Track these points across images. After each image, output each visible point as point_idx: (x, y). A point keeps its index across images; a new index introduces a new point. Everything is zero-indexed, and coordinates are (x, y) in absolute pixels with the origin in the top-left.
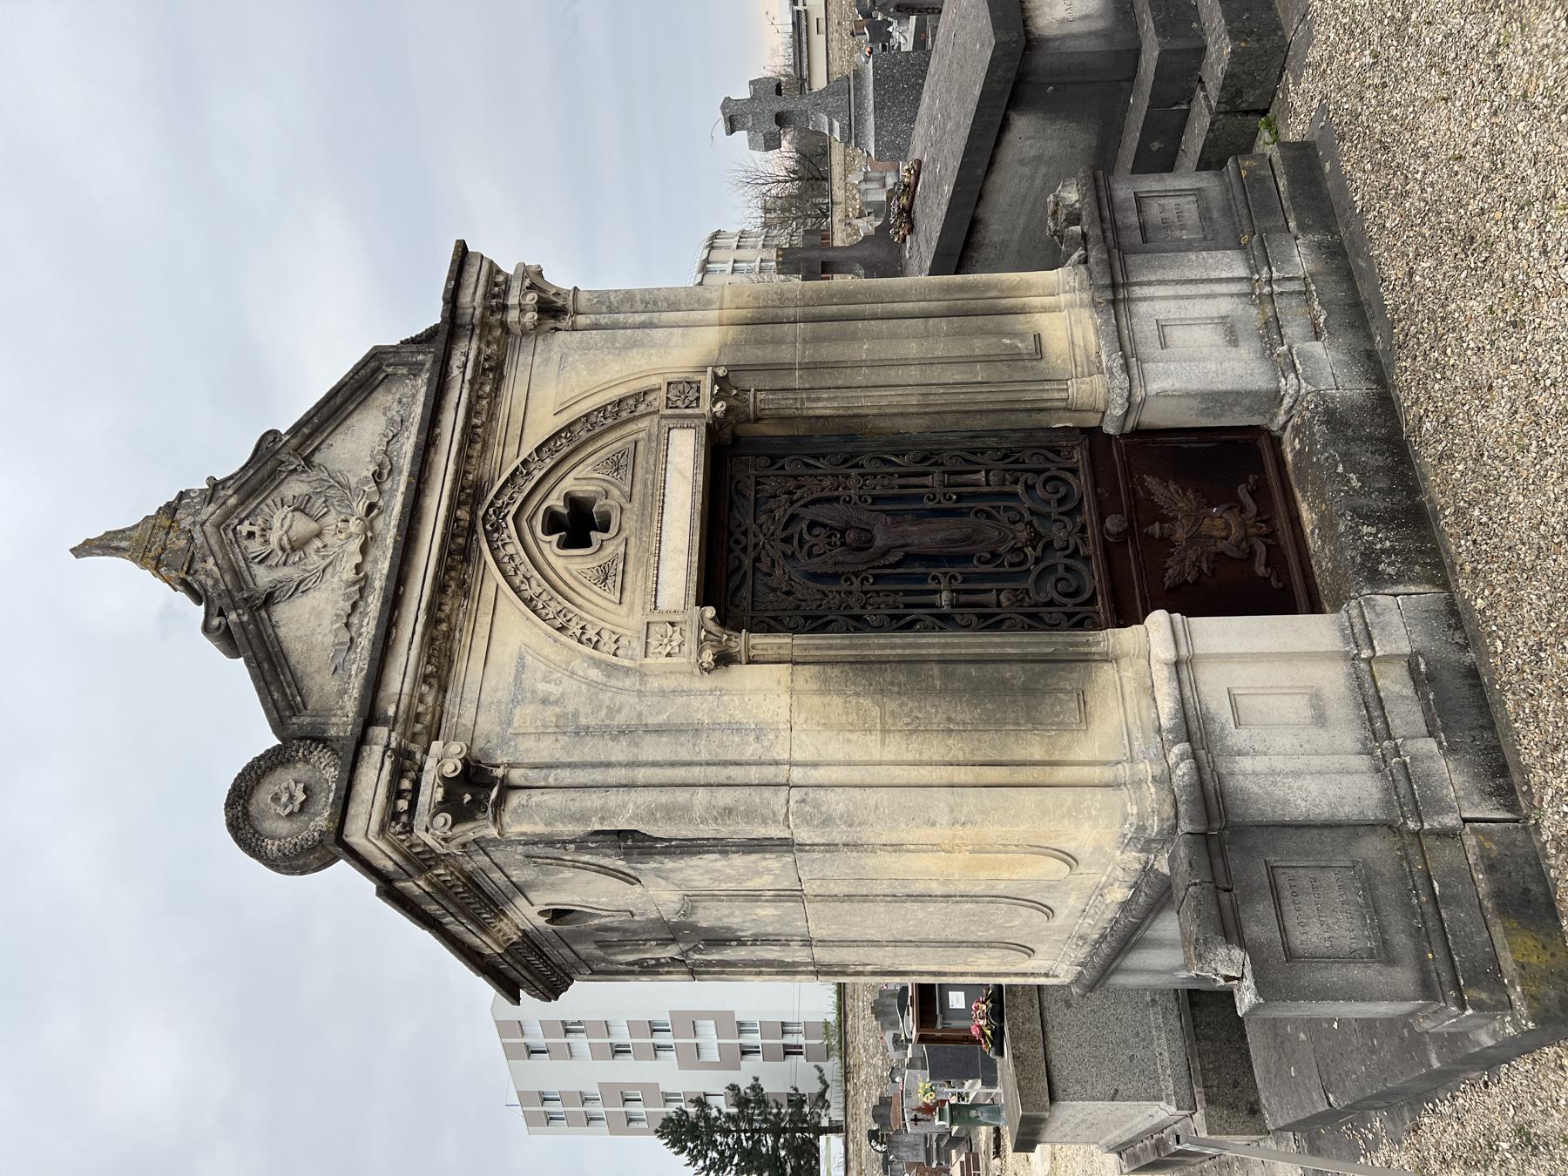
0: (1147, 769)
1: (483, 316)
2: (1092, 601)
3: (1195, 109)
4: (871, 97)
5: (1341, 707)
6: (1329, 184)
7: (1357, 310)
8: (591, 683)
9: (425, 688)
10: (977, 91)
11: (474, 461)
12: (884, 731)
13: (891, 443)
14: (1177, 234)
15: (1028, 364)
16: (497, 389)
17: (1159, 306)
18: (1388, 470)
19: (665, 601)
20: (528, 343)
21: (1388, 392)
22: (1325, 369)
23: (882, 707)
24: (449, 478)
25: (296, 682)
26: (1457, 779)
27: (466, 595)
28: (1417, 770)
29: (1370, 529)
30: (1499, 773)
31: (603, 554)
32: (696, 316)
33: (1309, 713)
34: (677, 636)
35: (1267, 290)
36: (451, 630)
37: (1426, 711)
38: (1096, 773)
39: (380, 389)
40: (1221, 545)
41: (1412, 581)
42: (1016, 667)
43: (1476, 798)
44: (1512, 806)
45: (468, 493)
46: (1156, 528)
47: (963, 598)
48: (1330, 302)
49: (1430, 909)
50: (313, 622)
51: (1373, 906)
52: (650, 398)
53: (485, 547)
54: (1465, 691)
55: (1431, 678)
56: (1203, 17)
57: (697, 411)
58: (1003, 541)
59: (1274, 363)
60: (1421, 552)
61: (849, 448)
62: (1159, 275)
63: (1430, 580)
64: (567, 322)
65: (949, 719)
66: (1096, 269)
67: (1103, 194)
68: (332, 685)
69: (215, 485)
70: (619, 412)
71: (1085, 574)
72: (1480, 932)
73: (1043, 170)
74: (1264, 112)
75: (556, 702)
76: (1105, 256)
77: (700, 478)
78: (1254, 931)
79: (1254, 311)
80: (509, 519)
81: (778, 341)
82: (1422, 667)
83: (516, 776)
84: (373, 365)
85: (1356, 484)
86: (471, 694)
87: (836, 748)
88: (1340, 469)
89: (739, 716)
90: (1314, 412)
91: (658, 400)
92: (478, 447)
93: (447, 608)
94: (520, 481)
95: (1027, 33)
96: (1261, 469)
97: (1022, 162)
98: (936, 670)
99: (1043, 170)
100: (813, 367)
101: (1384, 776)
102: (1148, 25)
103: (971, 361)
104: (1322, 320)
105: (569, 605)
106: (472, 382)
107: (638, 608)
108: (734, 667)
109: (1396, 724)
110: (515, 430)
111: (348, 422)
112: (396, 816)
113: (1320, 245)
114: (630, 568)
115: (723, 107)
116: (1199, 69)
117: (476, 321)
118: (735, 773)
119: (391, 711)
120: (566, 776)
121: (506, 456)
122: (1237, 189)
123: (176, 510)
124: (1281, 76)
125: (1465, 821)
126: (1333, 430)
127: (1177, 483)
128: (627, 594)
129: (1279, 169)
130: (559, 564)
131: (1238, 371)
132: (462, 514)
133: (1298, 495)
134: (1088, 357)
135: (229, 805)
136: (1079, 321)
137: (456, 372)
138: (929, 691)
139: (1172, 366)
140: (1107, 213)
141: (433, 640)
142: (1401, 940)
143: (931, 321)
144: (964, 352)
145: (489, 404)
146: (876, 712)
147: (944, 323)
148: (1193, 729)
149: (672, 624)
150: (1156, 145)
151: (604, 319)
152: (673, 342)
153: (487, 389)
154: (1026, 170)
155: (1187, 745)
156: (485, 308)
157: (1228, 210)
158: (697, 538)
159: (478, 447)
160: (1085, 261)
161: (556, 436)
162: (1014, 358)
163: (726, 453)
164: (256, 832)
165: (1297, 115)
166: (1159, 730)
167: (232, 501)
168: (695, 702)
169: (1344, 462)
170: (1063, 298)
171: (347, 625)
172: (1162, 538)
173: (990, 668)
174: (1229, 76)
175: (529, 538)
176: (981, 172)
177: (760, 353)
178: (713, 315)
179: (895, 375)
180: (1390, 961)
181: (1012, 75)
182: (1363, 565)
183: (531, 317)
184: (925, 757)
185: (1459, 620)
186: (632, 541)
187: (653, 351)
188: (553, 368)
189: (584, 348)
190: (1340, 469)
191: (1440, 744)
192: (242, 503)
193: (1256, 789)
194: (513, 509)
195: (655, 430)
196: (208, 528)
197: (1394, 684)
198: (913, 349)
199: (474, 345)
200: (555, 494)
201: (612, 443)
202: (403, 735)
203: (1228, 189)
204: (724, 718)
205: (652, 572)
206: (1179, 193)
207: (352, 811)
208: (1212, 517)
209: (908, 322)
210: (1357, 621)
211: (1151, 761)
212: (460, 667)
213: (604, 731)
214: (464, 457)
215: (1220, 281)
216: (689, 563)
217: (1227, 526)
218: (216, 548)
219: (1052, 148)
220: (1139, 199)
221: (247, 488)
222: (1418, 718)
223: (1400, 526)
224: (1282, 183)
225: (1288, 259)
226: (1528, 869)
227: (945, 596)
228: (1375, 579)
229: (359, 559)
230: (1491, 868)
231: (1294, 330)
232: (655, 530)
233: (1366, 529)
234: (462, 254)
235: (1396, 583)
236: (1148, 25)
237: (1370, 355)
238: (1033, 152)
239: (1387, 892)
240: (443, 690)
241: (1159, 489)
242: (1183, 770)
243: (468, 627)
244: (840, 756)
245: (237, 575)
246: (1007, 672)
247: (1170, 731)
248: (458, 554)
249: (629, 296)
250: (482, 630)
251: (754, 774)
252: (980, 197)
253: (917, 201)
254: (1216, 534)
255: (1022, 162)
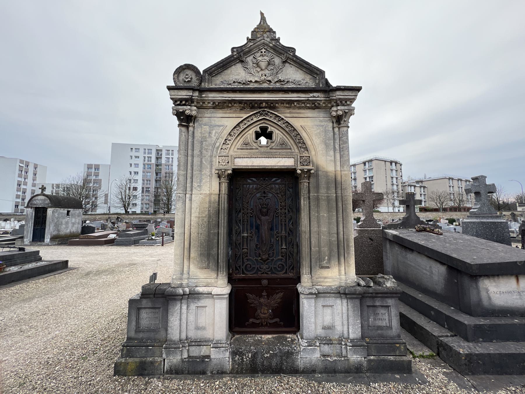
0: (185, 282)
1: (333, 99)
2: (243, 273)
3: (444, 330)
4: (488, 221)
5: (200, 335)
6: (390, 375)
7: (331, 371)
8: (215, 144)
9: (212, 103)
10: (454, 255)
11: (282, 105)
12: (199, 217)
13: (296, 222)
14: (372, 317)
15: (318, 264)
16: (309, 108)
17: (340, 307)
18: (270, 366)
19: (237, 160)
20: (328, 115)
21: (299, 373)
22: (308, 356)
23: (205, 217)
24: (274, 99)
25: (219, 73)
26: (175, 361)
27: (241, 110)
28: (178, 351)
29: (250, 356)
30: (176, 372)
31: (253, 143)
32: (338, 163)
33: (201, 326)
34: (224, 164)
35: (343, 343)
36: (230, 107)
37: (196, 357)
38: (186, 269)
39: (311, 77)
40: (259, 311)
41: (233, 364)
42: (216, 252)
43: (170, 364)
44: (167, 373)
45: (272, 105)
46: (264, 294)
47: (245, 239)
48: (336, 363)
49: (145, 345)
50: (237, 74)
51: (149, 330)
52: (306, 152)
53: (255, 112)
54: (199, 369)
55: (203, 361)
56: (484, 344)
57: (299, 165)
58: (263, 252)
59: (313, 340)
60: (242, 369)
61: (294, 210)
62: (350, 309)
63: (233, 369)
64: (335, 125)
65: (201, 234)
66: (353, 289)
67: (389, 295)
68: (218, 82)
69: (278, 40)
70: (301, 143)
71: (252, 273)
72: (139, 355)
73: (428, 274)
74: (438, 354)
75: (209, 136)
76: (357, 293)
77: (277, 167)
78: (144, 301)
79: (337, 337)
80: (264, 117)
81: (328, 188)
82: (207, 360)
83: (191, 129)
84: (318, 72)
85: (266, 355)
86: (213, 115)
87: (195, 205)
88: (271, 352)
89: (204, 181)
90: (293, 349)
91: (305, 154)
92: (287, 106)
93: (235, 105)
94: (277, 119)
95: (481, 276)
96: (285, 326)
97: (430, 267)
98: (216, 231)
99: (428, 274)
100: (318, 199)
101: (178, 342)
102: (482, 321)
103: (319, 246)
104: (329, 359)
105: (236, 135)
106: (308, 100)
107: (235, 153)
108: (218, 179)
109: (192, 349)
110: (296, 115)
111: (299, 70)
112: (181, 102)
113: (361, 365)
114: (249, 150)
115: (482, 176)
116: (460, 336)
117: (331, 98)
118: (189, 180)
119: (203, 96)
120: (190, 140)
121: (286, 115)
122: (391, 341)
123: (269, 32)
124: (451, 367)
125: (164, 360)
126: (285, 353)
127: (280, 302)
128: (240, 150)
129: (398, 358)
130: (250, 132)
131: (310, 328)
132: (264, 104)
133: (275, 336)
134: (320, 282)
135: (185, 65)
136: (334, 281)
137: (311, 95)
138: (209, 229)
139: (313, 308)
140: (380, 295)
141: (225, 103)
142: (141, 335)
143: (336, 235)
144: (322, 245)
145: (303, 107)
146: (204, 215)
147: (334, 239)
148: (193, 296)
149: (228, 162)
150: (433, 313)
151: (337, 136)
152: (328, 157)
153: (308, 105)
154: (428, 268)
155: (188, 293)
156: (336, 100)
157: (382, 336)
158: (256, 167)
159: (287, 106)
160: (359, 285)
161: (292, 126)
162: (320, 259)
163: (289, 175)
164: (180, 72)
165: (430, 369)
166: (196, 286)
167: (271, 45)
168: (208, 170)
169: (274, 353)
170: (343, 277)
171: (234, 82)
172: (262, 295)
173: (216, 245)
174: (451, 348)
175: (258, 123)
176: (426, 253)
177: (323, 183)
178: (338, 168)
179: (314, 224)
180: (136, 332)
181: (459, 269)
182: (239, 351)
183: (334, 114)
184: (192, 227)
185: (220, 374)
186: (257, 150)
187: (324, 152)
188: (319, 123)
189: (326, 131)
190: (271, 352)
191: (185, 358)
192: (271, 48)
193: (176, 308)
194: (268, 118)
195: (294, 154)
196: (263, 41)
197: (204, 351)
198: (324, 229)
199: (322, 99)
200: (272, 128)
201: (290, 142)
202: (197, 100)
203: (392, 338)
204: (203, 177)
205: (246, 156)
206: (390, 321)
207: (175, 91)
208: (268, 310)
209: (336, 228)
210: (221, 345)
211: (188, 283)
212: (220, 111)
213: (201, 148)
214: (282, 102)
215: (348, 328)
216: (249, 166)
217: (265, 314)
218: (256, 44)
219: (436, 278)
220: (388, 307)
221: (275, 48)
222: (194, 354)
223: (251, 365)
224: (392, 358)
225: (355, 353)
226: (151, 372)
227: (246, 235)
228: (234, 354)
229: (253, 81)
230: (152, 363)
231: (326, 349)
232: (259, 156)
233: (250, 355)
234: (358, 89)
235: (232, 359)
236: (482, 321)
237: (314, 371)
238: (434, 272)
239: (152, 335)
240: (214, 108)
241: (278, 297)
242: (180, 291)
243: (232, 111)
244: (193, 206)
245: (249, 51)
246: (215, 250)
247: (194, 289)
248: (252, 105)
249: (347, 142)
250: (231, 115)
251: (189, 185)
252: (419, 253)
253: (427, 233)
254: (262, 310)
255: (430, 267)
